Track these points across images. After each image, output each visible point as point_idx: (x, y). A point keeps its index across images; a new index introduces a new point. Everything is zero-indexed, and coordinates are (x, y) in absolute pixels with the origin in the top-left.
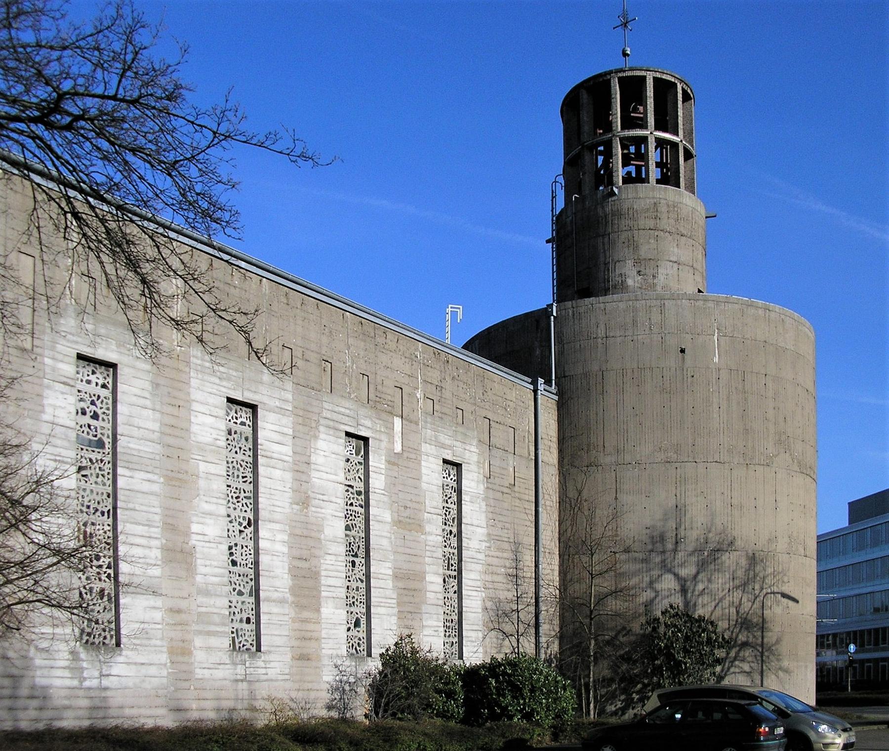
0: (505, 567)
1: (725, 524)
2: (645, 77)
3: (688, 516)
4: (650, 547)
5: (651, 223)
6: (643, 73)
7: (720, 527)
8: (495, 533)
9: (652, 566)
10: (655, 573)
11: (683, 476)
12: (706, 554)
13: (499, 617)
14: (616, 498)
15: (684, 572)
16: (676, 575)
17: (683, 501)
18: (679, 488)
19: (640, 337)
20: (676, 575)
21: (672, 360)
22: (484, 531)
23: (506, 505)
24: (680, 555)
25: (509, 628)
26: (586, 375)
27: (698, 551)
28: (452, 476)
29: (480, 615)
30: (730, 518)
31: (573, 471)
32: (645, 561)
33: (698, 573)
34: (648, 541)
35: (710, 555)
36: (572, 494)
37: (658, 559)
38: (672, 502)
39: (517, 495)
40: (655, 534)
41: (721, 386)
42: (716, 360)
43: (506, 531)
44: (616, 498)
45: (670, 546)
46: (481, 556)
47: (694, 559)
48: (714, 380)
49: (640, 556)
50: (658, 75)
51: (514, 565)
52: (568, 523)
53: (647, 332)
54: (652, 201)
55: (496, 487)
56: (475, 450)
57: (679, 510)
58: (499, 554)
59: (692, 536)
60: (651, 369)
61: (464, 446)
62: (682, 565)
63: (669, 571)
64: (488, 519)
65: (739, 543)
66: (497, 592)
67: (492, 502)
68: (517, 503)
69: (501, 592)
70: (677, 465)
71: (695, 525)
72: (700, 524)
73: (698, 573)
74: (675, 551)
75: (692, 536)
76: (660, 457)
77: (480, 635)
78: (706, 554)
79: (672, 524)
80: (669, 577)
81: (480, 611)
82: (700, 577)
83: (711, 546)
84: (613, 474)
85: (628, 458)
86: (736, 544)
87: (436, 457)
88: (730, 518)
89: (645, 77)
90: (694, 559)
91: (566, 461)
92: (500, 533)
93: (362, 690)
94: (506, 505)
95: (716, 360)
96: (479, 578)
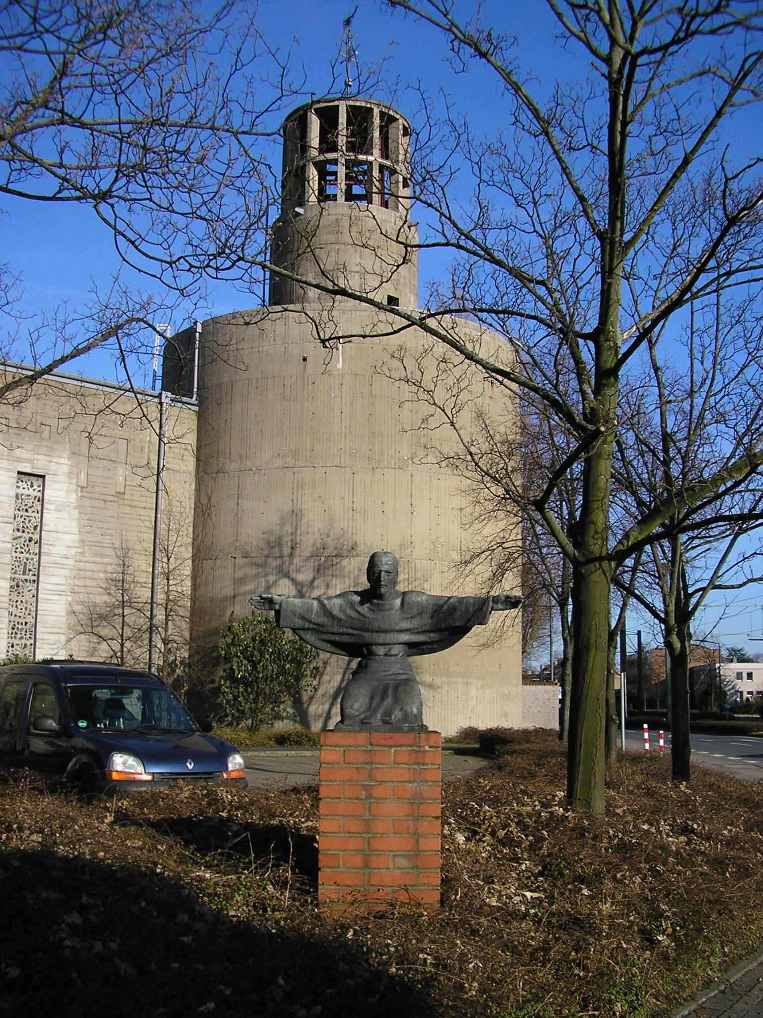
0: (105, 572)
1: (345, 529)
2: (338, 106)
3: (304, 521)
4: (266, 552)
5: (332, 238)
6: (336, 103)
7: (339, 532)
8: (92, 539)
9: (268, 570)
10: (272, 578)
11: (300, 481)
12: (323, 559)
13: (92, 621)
14: (238, 504)
15: (300, 577)
16: (293, 580)
17: (299, 506)
18: (295, 493)
19: (265, 348)
20: (293, 580)
21: (294, 368)
22: (77, 537)
23: (109, 513)
24: (296, 560)
25: (105, 632)
26: (220, 385)
27: (314, 555)
28: (35, 487)
29: (64, 619)
30: (351, 523)
31: (206, 477)
32: (264, 565)
33: (314, 579)
34: (264, 546)
35: (326, 561)
36: (204, 500)
37: (275, 563)
38: (288, 507)
39: (127, 502)
40: (271, 539)
41: (344, 391)
42: (339, 366)
43: (108, 537)
44: (238, 504)
45: (286, 551)
46: (71, 562)
47: (311, 564)
48: (337, 387)
49: (259, 561)
50: (351, 103)
51: (120, 570)
52: (200, 528)
53: (272, 343)
54: (334, 217)
55: (97, 496)
56: (66, 461)
57: (295, 515)
58: (94, 559)
59: (308, 542)
60: (273, 377)
61: (49, 459)
62: (298, 570)
63: (287, 575)
64: (81, 526)
65: (361, 548)
66: (91, 596)
67: (89, 510)
68: (127, 510)
69: (97, 597)
70: (295, 470)
71: (311, 530)
72: (316, 529)
73: (314, 579)
74: (291, 555)
75: (308, 542)
76: (279, 462)
77: (63, 638)
78: (323, 559)
79: (288, 529)
80: (286, 582)
81: (64, 614)
82: (316, 583)
83: (330, 551)
84: (237, 480)
85: (249, 464)
86: (358, 549)
87: (8, 470)
88: (351, 523)
89: (338, 106)
90: (311, 564)
91: (201, 468)
92: (99, 539)
93: (505, 690)
94: (109, 513)
95: (339, 366)
96: (63, 582)
